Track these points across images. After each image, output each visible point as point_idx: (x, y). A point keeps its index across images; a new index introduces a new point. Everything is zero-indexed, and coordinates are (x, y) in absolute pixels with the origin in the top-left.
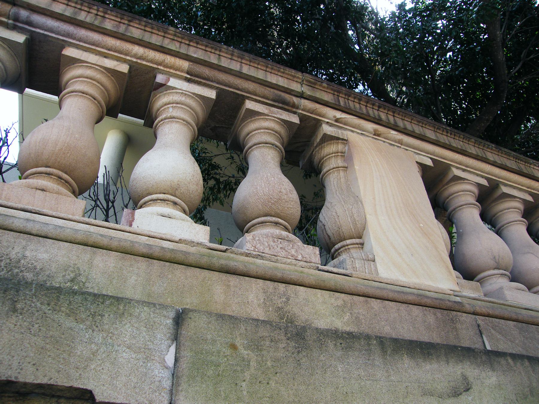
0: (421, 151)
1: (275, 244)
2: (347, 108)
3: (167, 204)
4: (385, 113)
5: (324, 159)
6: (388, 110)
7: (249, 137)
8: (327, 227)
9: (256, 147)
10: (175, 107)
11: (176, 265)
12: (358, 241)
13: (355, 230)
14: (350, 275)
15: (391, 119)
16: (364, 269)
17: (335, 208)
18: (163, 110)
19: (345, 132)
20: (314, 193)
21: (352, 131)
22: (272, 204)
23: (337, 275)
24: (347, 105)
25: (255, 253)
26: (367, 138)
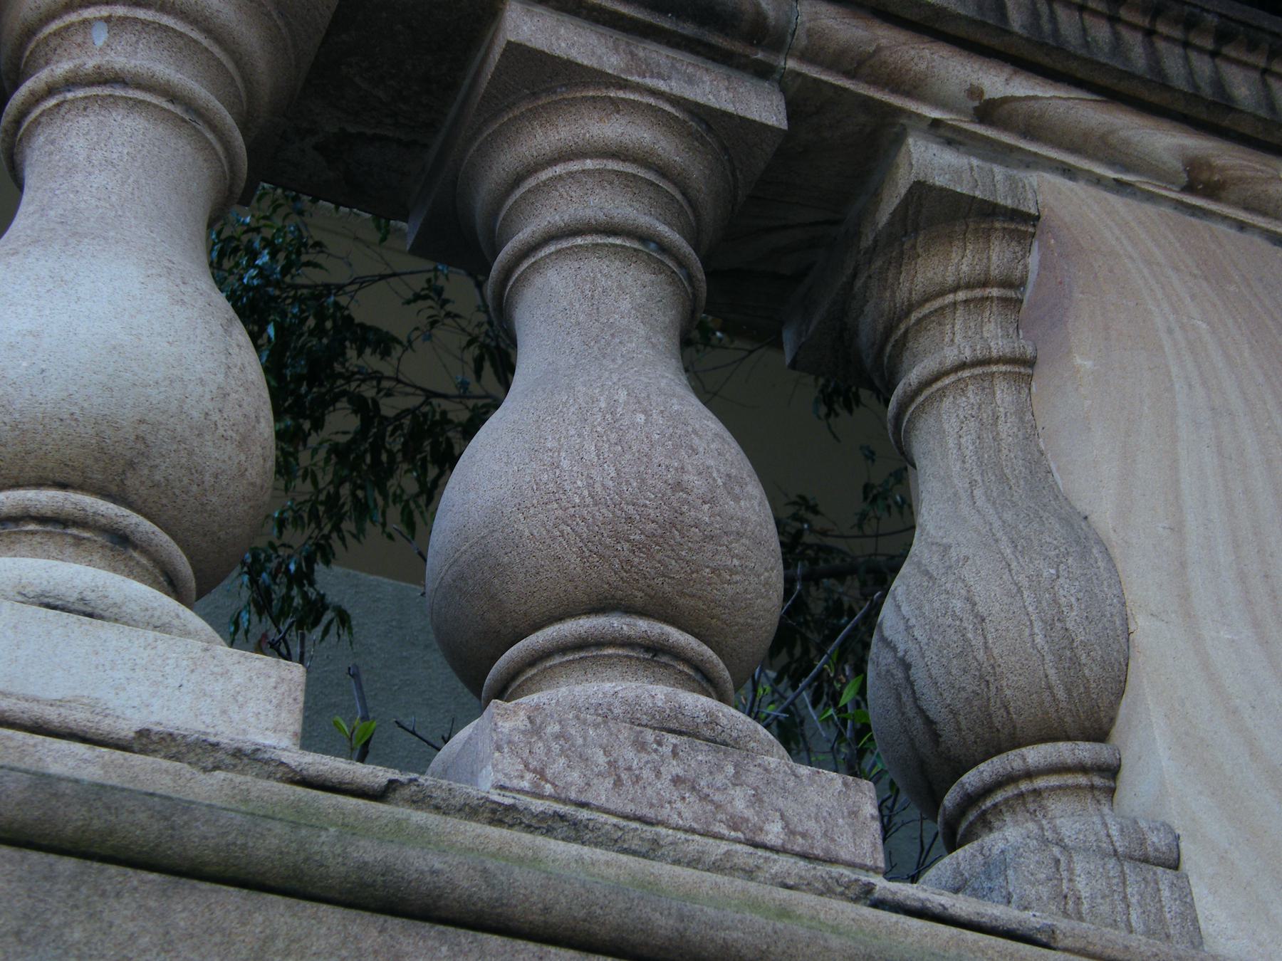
1: (645, 757)
2: (1042, 45)
3: (78, 541)
4: (1254, 67)
5: (914, 317)
7: (523, 197)
8: (918, 674)
9: (558, 252)
10: (123, 20)
11: (113, 870)
12: (1084, 751)
13: (1069, 691)
14: (1044, 938)
16: (1120, 907)
17: (966, 572)
18: (56, 34)
20: (867, 488)
21: (1068, 172)
22: (636, 547)
24: (1047, 27)
25: (538, 805)
26: (1149, 209)
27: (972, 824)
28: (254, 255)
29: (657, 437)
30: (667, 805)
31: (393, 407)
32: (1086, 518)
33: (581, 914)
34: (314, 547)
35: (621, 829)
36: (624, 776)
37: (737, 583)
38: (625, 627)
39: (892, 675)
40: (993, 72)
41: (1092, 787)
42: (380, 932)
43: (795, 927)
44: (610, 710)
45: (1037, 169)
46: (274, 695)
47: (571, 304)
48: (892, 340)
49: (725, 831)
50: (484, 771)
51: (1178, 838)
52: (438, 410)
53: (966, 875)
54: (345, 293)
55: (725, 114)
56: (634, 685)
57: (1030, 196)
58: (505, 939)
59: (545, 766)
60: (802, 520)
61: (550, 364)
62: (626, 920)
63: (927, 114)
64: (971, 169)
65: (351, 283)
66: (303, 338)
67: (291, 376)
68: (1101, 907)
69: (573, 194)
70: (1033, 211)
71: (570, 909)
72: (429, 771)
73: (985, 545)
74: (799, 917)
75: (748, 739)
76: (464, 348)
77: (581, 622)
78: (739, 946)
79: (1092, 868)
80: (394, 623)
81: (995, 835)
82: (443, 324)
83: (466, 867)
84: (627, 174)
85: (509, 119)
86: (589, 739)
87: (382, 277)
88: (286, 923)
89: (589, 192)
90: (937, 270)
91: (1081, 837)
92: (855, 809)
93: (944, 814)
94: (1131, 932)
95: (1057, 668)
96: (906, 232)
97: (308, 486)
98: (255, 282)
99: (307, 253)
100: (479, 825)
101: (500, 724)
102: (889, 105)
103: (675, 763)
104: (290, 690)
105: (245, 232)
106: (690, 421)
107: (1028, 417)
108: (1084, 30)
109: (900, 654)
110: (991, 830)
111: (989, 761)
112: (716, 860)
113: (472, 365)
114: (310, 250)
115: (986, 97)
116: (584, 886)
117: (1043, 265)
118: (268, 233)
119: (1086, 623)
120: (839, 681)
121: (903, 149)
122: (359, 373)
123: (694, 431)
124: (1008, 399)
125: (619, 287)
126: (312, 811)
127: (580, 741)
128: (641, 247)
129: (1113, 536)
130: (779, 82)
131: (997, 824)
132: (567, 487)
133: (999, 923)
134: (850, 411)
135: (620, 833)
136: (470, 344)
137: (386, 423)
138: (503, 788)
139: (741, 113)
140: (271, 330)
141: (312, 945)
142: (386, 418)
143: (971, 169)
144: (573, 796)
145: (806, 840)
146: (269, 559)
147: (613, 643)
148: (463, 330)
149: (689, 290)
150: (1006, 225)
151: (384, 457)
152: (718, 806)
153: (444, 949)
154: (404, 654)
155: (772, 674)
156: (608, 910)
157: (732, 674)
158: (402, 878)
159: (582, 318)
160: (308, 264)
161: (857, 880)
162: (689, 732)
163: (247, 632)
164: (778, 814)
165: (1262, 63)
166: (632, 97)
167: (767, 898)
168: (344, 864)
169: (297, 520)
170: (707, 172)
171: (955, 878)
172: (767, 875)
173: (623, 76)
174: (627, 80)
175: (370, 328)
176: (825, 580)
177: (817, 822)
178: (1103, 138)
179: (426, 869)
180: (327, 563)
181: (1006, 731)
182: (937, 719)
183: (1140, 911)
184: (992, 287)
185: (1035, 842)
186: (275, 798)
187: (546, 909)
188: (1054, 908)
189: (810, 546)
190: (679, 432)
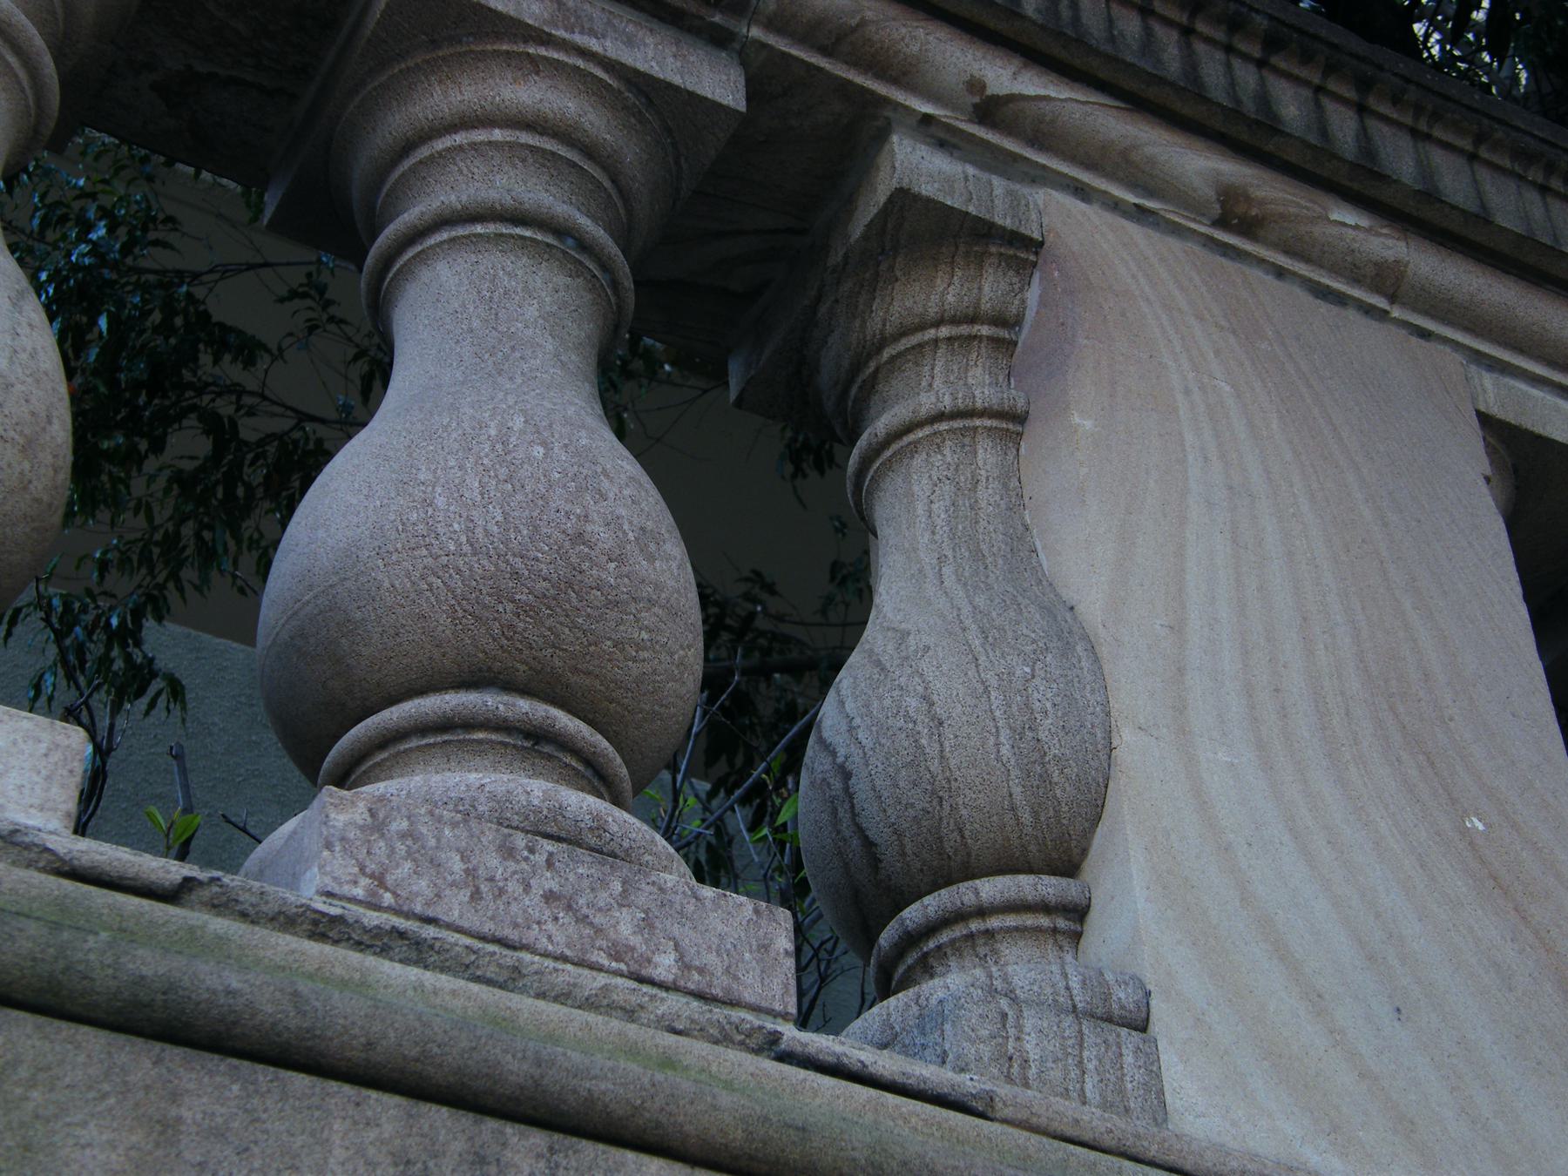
0: (1519, 349)
1: (512, 866)
5: (887, 353)
6: (1330, 69)
7: (413, 170)
8: (860, 786)
9: (453, 240)
12: (1049, 887)
13: (1035, 814)
15: (1344, 125)
19: (1042, 196)
20: (835, 567)
21: (1081, 192)
22: (522, 609)
23: (891, 1099)
25: (372, 918)
26: (1174, 243)
27: (910, 968)
28: (88, 227)
29: (557, 476)
30: (535, 926)
31: (255, 429)
32: (1072, 608)
33: (413, 1053)
34: (143, 598)
35: (474, 952)
36: (484, 888)
37: (644, 661)
38: (501, 707)
39: (829, 785)
40: (999, 62)
41: (1055, 931)
42: (155, 1063)
43: (678, 1080)
44: (474, 806)
45: (1045, 185)
46: (44, 763)
47: (464, 306)
48: (859, 380)
49: (606, 962)
50: (308, 874)
51: (1148, 994)
52: (312, 437)
53: (897, 1029)
54: (202, 284)
55: (670, 86)
56: (505, 778)
57: (1034, 216)
58: (314, 1078)
59: (386, 870)
60: (755, 601)
61: (432, 378)
62: (470, 1062)
63: (917, 108)
64: (966, 179)
65: (211, 271)
66: (144, 336)
67: (126, 382)
68: (1052, 1073)
69: (476, 170)
70: (1036, 235)
71: (401, 1045)
72: (243, 871)
73: (951, 634)
74: (687, 1068)
75: (642, 851)
76: (350, 362)
77: (447, 697)
78: (607, 1099)
79: (1045, 1025)
80: (243, 699)
81: (936, 981)
82: (325, 331)
83: (272, 988)
84: (544, 151)
85: (401, 71)
86: (444, 841)
87: (250, 267)
88: (34, 1047)
89: (496, 169)
90: (917, 298)
91: (1035, 988)
92: (766, 942)
93: (879, 955)
94: (1084, 1103)
95: (1024, 787)
96: (883, 250)
97: (141, 521)
98: (87, 261)
99: (156, 229)
100: (296, 939)
101: (332, 816)
102: (872, 93)
103: (548, 874)
104: (66, 759)
105: (77, 198)
106: (601, 460)
107: (1014, 483)
108: (1110, 21)
109: (840, 760)
110: (932, 977)
111: (936, 893)
112: (590, 996)
113: (358, 382)
114: (160, 227)
115: (989, 92)
116: (419, 1018)
117: (1043, 303)
118: (107, 201)
119: (1061, 734)
120: (779, 795)
121: (887, 147)
122: (214, 384)
123: (605, 473)
124: (992, 460)
125: (526, 289)
126: (81, 910)
127: (432, 842)
128: (555, 243)
129: (1101, 631)
130: (740, 53)
131: (939, 969)
132: (441, 530)
133: (929, 1086)
134: (822, 473)
135: (473, 957)
136: (356, 358)
137: (245, 449)
138: (330, 894)
139: (690, 88)
140: (103, 323)
141: (65, 1075)
142: (246, 443)
143: (966, 179)
144: (418, 909)
145: (703, 977)
146: (84, 610)
147: (485, 725)
148: (350, 339)
149: (613, 299)
150: (1002, 250)
151: (240, 491)
152: (599, 931)
153: (235, 1088)
154: (254, 738)
155: (704, 786)
156: (447, 1049)
157: (631, 773)
158: (189, 998)
159: (476, 324)
160: (156, 243)
161: (761, 1028)
162: (570, 837)
163: (50, 699)
164: (672, 943)
165: (1316, 79)
166: (556, 56)
167: (649, 1043)
168: (115, 978)
169: (125, 561)
170: (645, 156)
171: (882, 1032)
172: (652, 1017)
173: (546, 29)
174: (550, 35)
175: (231, 329)
176: (777, 676)
177: (719, 954)
178: (1125, 154)
179: (220, 988)
180: (160, 619)
181: (959, 858)
182: (879, 841)
183: (1096, 1078)
184: (982, 324)
185: (980, 991)
186: (34, 892)
187: (369, 1044)
188: (995, 1071)
189: (762, 634)
190: (585, 472)
